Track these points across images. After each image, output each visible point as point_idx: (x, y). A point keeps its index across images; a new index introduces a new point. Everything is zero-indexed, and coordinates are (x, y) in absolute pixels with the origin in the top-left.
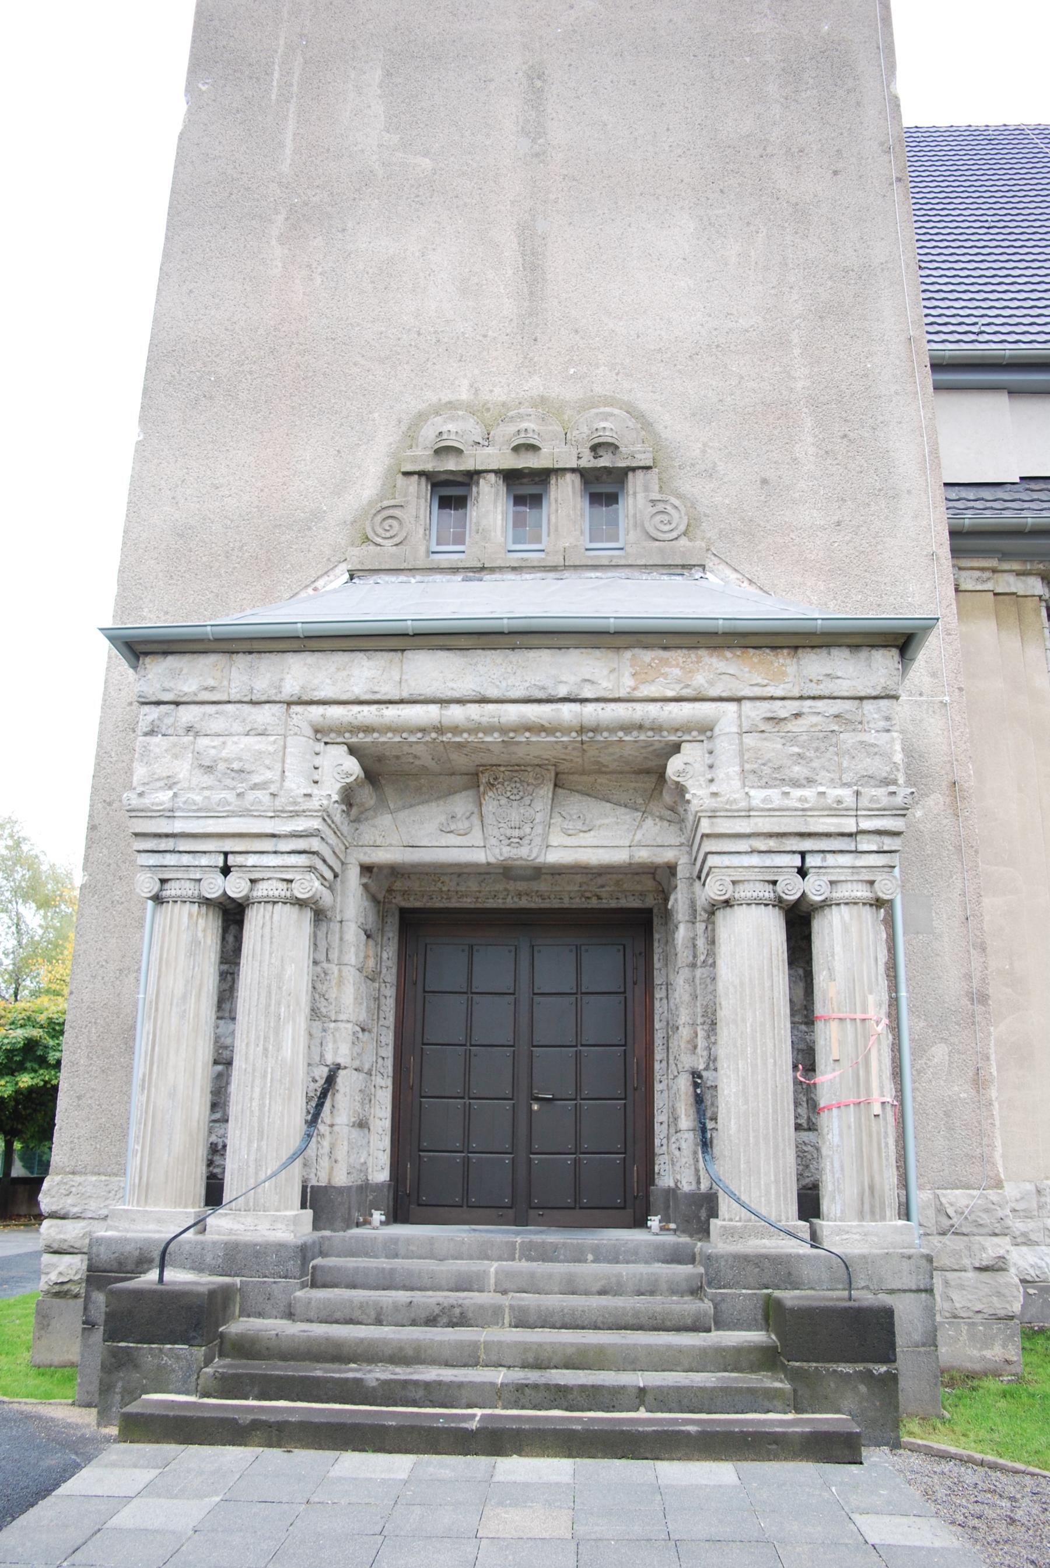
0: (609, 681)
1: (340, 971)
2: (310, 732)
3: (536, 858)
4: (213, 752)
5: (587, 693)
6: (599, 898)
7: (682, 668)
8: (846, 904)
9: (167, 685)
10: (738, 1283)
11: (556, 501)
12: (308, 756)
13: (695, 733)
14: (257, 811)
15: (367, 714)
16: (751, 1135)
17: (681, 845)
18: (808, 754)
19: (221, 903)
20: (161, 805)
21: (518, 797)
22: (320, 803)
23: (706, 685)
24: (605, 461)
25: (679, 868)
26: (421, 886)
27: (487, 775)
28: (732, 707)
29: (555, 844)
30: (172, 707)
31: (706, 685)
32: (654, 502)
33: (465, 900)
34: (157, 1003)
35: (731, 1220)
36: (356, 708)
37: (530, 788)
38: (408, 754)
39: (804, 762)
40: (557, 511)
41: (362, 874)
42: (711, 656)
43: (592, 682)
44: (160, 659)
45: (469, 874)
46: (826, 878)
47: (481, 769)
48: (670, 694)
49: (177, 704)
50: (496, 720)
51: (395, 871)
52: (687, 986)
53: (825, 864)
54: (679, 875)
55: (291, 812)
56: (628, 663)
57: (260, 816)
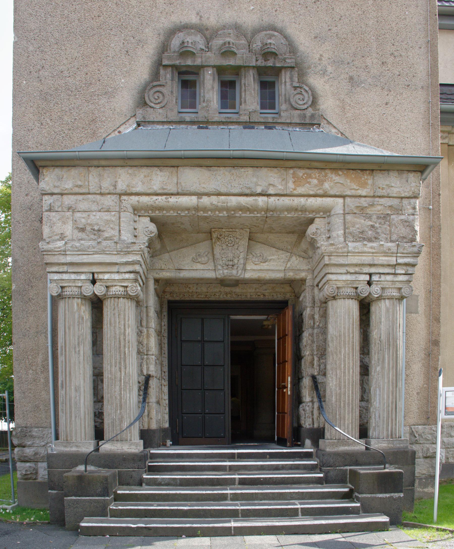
0: (282, 185)
1: (148, 331)
2: (131, 210)
3: (240, 275)
4: (83, 220)
5: (271, 191)
6: (264, 295)
7: (317, 179)
8: (388, 299)
9: (56, 184)
10: (335, 465)
11: (245, 85)
12: (131, 223)
13: (321, 213)
14: (108, 251)
15: (161, 200)
16: (342, 403)
17: (309, 269)
18: (376, 225)
19: (91, 298)
20: (59, 248)
21: (232, 245)
22: (140, 247)
23: (329, 189)
24: (270, 63)
25: (307, 281)
26: (179, 290)
27: (216, 233)
28: (341, 200)
29: (249, 269)
30: (60, 196)
31: (329, 189)
32: (295, 88)
33: (200, 296)
34: (65, 347)
35: (331, 439)
36: (155, 198)
37: (237, 240)
38: (179, 222)
39: (374, 229)
40: (245, 90)
41: (155, 284)
42: (332, 174)
43: (274, 186)
44: (51, 169)
45: (202, 284)
46: (379, 286)
47: (213, 230)
48: (311, 193)
49: (62, 194)
50: (225, 204)
51: (168, 282)
52: (310, 337)
53: (380, 280)
54: (307, 284)
55: (125, 251)
56: (291, 176)
57: (110, 254)
